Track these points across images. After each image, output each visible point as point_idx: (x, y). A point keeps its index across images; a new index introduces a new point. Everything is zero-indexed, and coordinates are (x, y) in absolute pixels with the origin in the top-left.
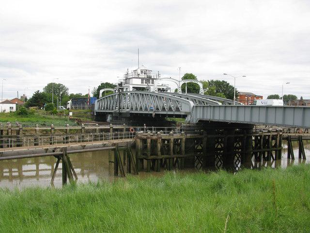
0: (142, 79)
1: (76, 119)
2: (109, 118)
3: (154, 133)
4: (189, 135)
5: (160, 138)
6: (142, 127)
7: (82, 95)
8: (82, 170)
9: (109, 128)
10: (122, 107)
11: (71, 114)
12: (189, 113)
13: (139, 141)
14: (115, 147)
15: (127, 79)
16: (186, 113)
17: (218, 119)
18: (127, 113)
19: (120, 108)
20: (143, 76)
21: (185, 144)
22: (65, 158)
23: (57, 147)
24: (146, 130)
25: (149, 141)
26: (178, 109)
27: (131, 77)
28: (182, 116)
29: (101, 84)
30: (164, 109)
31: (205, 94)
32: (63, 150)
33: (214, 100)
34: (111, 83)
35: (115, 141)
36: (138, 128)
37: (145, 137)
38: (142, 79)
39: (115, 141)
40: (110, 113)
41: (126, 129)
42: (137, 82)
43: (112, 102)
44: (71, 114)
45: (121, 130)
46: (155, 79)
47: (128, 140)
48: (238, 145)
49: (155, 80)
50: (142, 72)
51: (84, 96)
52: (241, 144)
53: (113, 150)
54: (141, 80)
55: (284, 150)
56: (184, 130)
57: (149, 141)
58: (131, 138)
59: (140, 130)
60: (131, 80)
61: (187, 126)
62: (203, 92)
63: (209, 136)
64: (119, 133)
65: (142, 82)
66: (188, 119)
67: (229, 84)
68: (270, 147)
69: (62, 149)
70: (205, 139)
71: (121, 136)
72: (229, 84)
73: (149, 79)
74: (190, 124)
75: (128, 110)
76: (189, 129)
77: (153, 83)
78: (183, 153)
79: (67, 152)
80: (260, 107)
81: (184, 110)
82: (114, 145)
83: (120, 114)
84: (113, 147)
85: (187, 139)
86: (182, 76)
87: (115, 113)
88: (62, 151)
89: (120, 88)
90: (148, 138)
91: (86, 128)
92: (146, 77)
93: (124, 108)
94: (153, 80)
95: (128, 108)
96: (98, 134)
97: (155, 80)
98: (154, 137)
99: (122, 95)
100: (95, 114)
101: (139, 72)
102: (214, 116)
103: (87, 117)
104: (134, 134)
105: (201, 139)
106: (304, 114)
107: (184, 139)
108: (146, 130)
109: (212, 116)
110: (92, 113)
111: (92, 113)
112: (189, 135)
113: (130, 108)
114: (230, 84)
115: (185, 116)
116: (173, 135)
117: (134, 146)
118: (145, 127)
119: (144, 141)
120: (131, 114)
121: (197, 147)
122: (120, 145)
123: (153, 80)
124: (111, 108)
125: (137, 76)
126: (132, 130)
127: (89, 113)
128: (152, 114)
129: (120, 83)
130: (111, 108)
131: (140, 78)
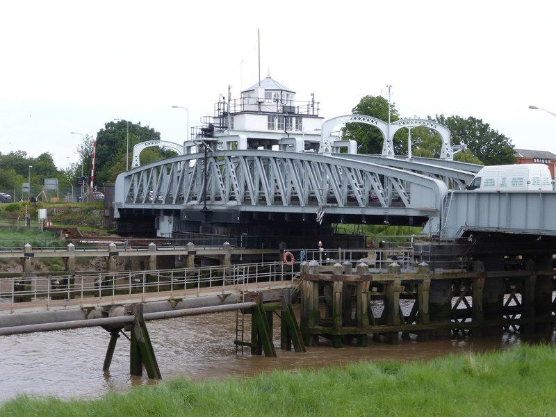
0: (271, 116)
1: (65, 231)
2: (166, 228)
3: (348, 266)
4: (439, 271)
5: (368, 278)
6: (313, 251)
7: (27, 157)
8: (419, 336)
9: (186, 253)
10: (212, 196)
11: (43, 214)
12: (434, 212)
13: (309, 286)
14: (254, 303)
15: (226, 117)
16: (422, 211)
17: (496, 225)
18: (230, 213)
19: (205, 197)
20: (272, 107)
21: (430, 295)
22: (138, 330)
23: (116, 303)
24: (324, 258)
25: (338, 286)
26: (397, 202)
27: (239, 109)
28: (411, 220)
29: (107, 127)
30: (294, 200)
31: (457, 158)
32: (135, 311)
33: (402, 169)
34: (135, 122)
35: (254, 288)
36: (303, 252)
37: (328, 277)
38: (271, 116)
39: (254, 288)
40: (168, 212)
41: (233, 256)
42: (257, 125)
43: (167, 178)
44: (43, 214)
45: (217, 261)
46: (308, 116)
47: (282, 285)
48: (462, 306)
49: (304, 119)
50: (268, 96)
51: (31, 161)
52: (470, 303)
53: (245, 311)
54: (267, 116)
55: (277, 338)
56: (425, 258)
57: (338, 286)
58: (288, 278)
59: (309, 257)
60: (236, 118)
61: (434, 248)
62: (452, 154)
63: (490, 274)
64: (211, 268)
65: (271, 126)
66: (431, 228)
67: (487, 125)
68: (397, 320)
69: (130, 310)
70: (481, 282)
71: (217, 279)
72: (487, 125)
73: (288, 115)
74: (438, 241)
75: (233, 203)
76: (440, 253)
77: (299, 127)
78: (426, 319)
79: (145, 315)
80: (489, 194)
81: (417, 202)
82: (252, 296)
83: (208, 214)
84: (249, 304)
85: (434, 282)
86: (356, 102)
87: (190, 212)
88: (130, 314)
89: (208, 142)
90: (337, 278)
91: (120, 254)
92: (280, 109)
93: (219, 199)
94: (300, 117)
95: (232, 199)
96: (154, 271)
97: (304, 119)
98: (352, 277)
99: (211, 160)
100: (117, 215)
101: (261, 94)
102: (526, 223)
103: (92, 224)
104: (297, 268)
105: (468, 282)
106: (509, 206)
107: (427, 281)
108: (324, 258)
109: (503, 216)
110: (107, 213)
111: (107, 213)
112: (439, 271)
113: (239, 197)
114: (492, 127)
115: (420, 221)
116: (399, 272)
117: (297, 297)
118: (322, 250)
119: (323, 285)
120: (244, 214)
121: (457, 305)
122: (266, 297)
123: (300, 117)
124: (144, 197)
125: (255, 108)
126: (289, 259)
127: (96, 213)
128: (314, 215)
129: (205, 126)
130: (144, 197)
131: (264, 113)
